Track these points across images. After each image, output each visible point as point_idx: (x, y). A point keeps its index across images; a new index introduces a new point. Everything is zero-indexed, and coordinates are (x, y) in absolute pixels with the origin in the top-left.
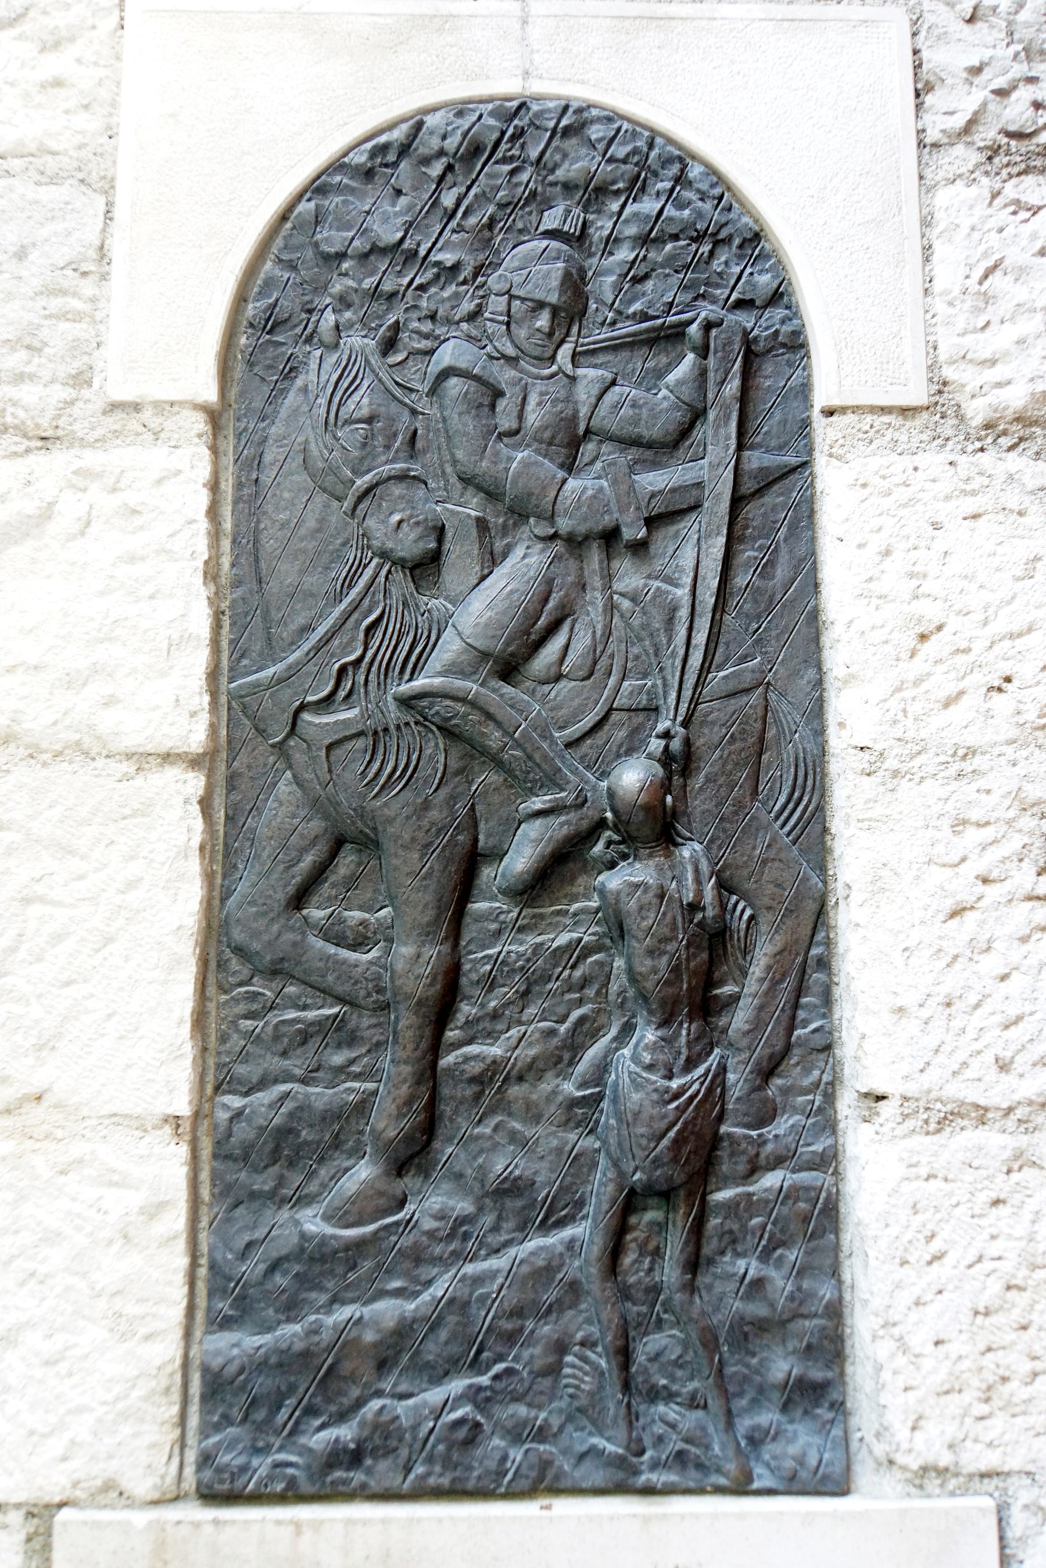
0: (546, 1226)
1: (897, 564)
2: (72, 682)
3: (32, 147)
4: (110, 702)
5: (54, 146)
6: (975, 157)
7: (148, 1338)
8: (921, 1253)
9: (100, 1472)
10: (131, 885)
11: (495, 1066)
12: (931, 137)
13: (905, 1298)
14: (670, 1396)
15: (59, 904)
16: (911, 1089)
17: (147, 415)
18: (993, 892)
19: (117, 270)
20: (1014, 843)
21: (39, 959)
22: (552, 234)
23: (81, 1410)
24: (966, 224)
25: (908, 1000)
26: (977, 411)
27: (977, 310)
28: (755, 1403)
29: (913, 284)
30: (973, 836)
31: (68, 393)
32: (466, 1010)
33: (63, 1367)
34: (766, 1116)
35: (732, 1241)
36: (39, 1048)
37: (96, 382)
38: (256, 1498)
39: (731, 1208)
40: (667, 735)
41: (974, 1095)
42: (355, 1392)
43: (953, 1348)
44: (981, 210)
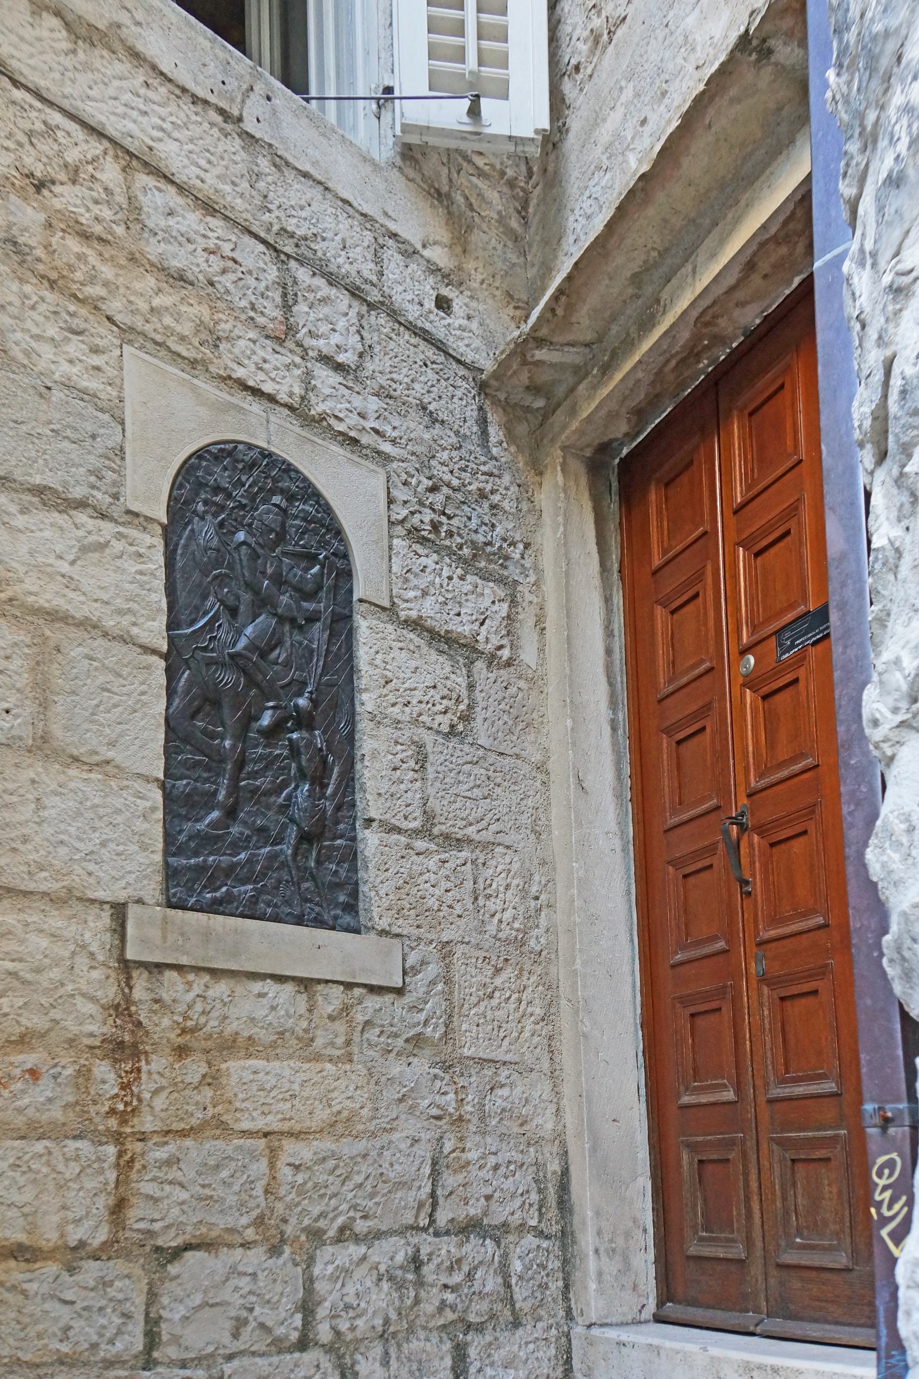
0: (273, 844)
1: (379, 656)
2: (120, 612)
3: (91, 392)
4: (134, 624)
5: (99, 395)
6: (405, 532)
7: (152, 852)
8: (383, 868)
9: (137, 894)
10: (143, 693)
11: (258, 788)
12: (393, 519)
13: (379, 880)
14: (311, 901)
15: (116, 694)
16: (382, 818)
17: (142, 519)
18: (405, 766)
19: (128, 456)
20: (410, 753)
21: (109, 712)
22: (275, 505)
23: (130, 872)
24: (402, 553)
25: (382, 791)
26: (403, 615)
27: (404, 583)
28: (335, 908)
29: (385, 566)
30: (399, 747)
31: (111, 500)
32: (248, 768)
33: (123, 857)
34: (337, 823)
35: (329, 858)
36: (109, 744)
37: (122, 499)
38: (192, 909)
39: (328, 847)
40: (311, 693)
41: (397, 823)
42: (218, 883)
43: (391, 897)
44: (406, 550)
